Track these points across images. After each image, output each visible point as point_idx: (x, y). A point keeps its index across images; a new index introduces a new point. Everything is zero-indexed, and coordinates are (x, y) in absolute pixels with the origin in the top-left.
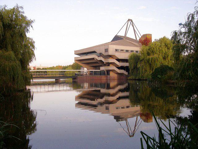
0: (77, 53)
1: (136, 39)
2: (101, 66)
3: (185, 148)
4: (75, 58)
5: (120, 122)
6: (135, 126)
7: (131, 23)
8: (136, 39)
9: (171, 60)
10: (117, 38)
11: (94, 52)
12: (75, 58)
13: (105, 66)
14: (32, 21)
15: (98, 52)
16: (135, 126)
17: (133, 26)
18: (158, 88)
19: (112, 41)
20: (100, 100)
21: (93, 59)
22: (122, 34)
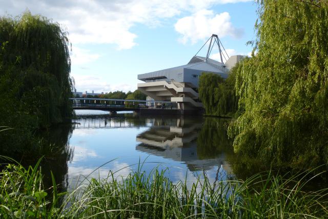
7: (217, 40)
8: (222, 61)
10: (195, 60)
11: (164, 78)
22: (202, 54)
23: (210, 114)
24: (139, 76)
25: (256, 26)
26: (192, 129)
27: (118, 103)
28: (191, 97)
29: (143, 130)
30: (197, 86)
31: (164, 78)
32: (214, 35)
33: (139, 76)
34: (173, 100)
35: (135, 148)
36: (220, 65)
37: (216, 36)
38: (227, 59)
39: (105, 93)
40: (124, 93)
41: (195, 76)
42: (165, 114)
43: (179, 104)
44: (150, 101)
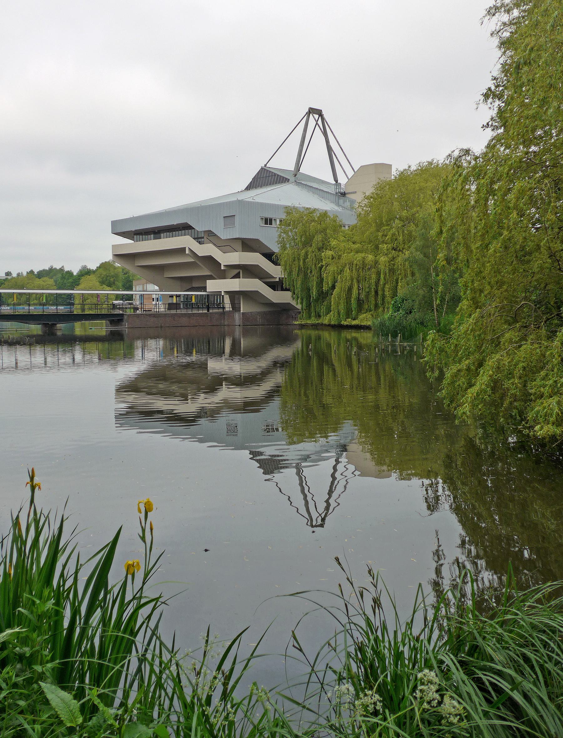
0: (121, 229)
1: (336, 181)
2: (211, 277)
3: (560, 545)
4: (114, 246)
5: (277, 477)
6: (330, 493)
7: (320, 122)
8: (336, 181)
9: (460, 244)
10: (266, 178)
11: (185, 228)
12: (114, 246)
13: (224, 278)
14: (63, 267)
15: (199, 227)
16: (330, 493)
17: (325, 134)
18: (506, 61)
19: (249, 188)
20: (203, 400)
21: (181, 251)
22: (284, 162)
23: (313, 321)
24: (114, 224)
25: (8, 274)
26: (264, 362)
27: (57, 300)
28: (260, 279)
29: (128, 371)
30: (275, 248)
31: (185, 228)
32: (312, 111)
33: (114, 224)
34: (212, 286)
35: (151, 500)
36: (332, 190)
37: (319, 113)
38: (350, 173)
39: (413, 168)
40: (70, 273)
41: (268, 221)
42: (196, 326)
43: (227, 300)
44: (150, 294)
